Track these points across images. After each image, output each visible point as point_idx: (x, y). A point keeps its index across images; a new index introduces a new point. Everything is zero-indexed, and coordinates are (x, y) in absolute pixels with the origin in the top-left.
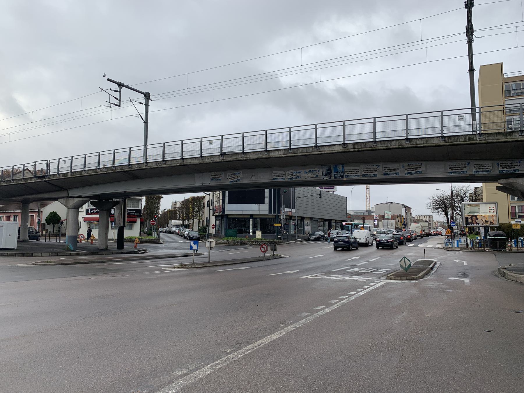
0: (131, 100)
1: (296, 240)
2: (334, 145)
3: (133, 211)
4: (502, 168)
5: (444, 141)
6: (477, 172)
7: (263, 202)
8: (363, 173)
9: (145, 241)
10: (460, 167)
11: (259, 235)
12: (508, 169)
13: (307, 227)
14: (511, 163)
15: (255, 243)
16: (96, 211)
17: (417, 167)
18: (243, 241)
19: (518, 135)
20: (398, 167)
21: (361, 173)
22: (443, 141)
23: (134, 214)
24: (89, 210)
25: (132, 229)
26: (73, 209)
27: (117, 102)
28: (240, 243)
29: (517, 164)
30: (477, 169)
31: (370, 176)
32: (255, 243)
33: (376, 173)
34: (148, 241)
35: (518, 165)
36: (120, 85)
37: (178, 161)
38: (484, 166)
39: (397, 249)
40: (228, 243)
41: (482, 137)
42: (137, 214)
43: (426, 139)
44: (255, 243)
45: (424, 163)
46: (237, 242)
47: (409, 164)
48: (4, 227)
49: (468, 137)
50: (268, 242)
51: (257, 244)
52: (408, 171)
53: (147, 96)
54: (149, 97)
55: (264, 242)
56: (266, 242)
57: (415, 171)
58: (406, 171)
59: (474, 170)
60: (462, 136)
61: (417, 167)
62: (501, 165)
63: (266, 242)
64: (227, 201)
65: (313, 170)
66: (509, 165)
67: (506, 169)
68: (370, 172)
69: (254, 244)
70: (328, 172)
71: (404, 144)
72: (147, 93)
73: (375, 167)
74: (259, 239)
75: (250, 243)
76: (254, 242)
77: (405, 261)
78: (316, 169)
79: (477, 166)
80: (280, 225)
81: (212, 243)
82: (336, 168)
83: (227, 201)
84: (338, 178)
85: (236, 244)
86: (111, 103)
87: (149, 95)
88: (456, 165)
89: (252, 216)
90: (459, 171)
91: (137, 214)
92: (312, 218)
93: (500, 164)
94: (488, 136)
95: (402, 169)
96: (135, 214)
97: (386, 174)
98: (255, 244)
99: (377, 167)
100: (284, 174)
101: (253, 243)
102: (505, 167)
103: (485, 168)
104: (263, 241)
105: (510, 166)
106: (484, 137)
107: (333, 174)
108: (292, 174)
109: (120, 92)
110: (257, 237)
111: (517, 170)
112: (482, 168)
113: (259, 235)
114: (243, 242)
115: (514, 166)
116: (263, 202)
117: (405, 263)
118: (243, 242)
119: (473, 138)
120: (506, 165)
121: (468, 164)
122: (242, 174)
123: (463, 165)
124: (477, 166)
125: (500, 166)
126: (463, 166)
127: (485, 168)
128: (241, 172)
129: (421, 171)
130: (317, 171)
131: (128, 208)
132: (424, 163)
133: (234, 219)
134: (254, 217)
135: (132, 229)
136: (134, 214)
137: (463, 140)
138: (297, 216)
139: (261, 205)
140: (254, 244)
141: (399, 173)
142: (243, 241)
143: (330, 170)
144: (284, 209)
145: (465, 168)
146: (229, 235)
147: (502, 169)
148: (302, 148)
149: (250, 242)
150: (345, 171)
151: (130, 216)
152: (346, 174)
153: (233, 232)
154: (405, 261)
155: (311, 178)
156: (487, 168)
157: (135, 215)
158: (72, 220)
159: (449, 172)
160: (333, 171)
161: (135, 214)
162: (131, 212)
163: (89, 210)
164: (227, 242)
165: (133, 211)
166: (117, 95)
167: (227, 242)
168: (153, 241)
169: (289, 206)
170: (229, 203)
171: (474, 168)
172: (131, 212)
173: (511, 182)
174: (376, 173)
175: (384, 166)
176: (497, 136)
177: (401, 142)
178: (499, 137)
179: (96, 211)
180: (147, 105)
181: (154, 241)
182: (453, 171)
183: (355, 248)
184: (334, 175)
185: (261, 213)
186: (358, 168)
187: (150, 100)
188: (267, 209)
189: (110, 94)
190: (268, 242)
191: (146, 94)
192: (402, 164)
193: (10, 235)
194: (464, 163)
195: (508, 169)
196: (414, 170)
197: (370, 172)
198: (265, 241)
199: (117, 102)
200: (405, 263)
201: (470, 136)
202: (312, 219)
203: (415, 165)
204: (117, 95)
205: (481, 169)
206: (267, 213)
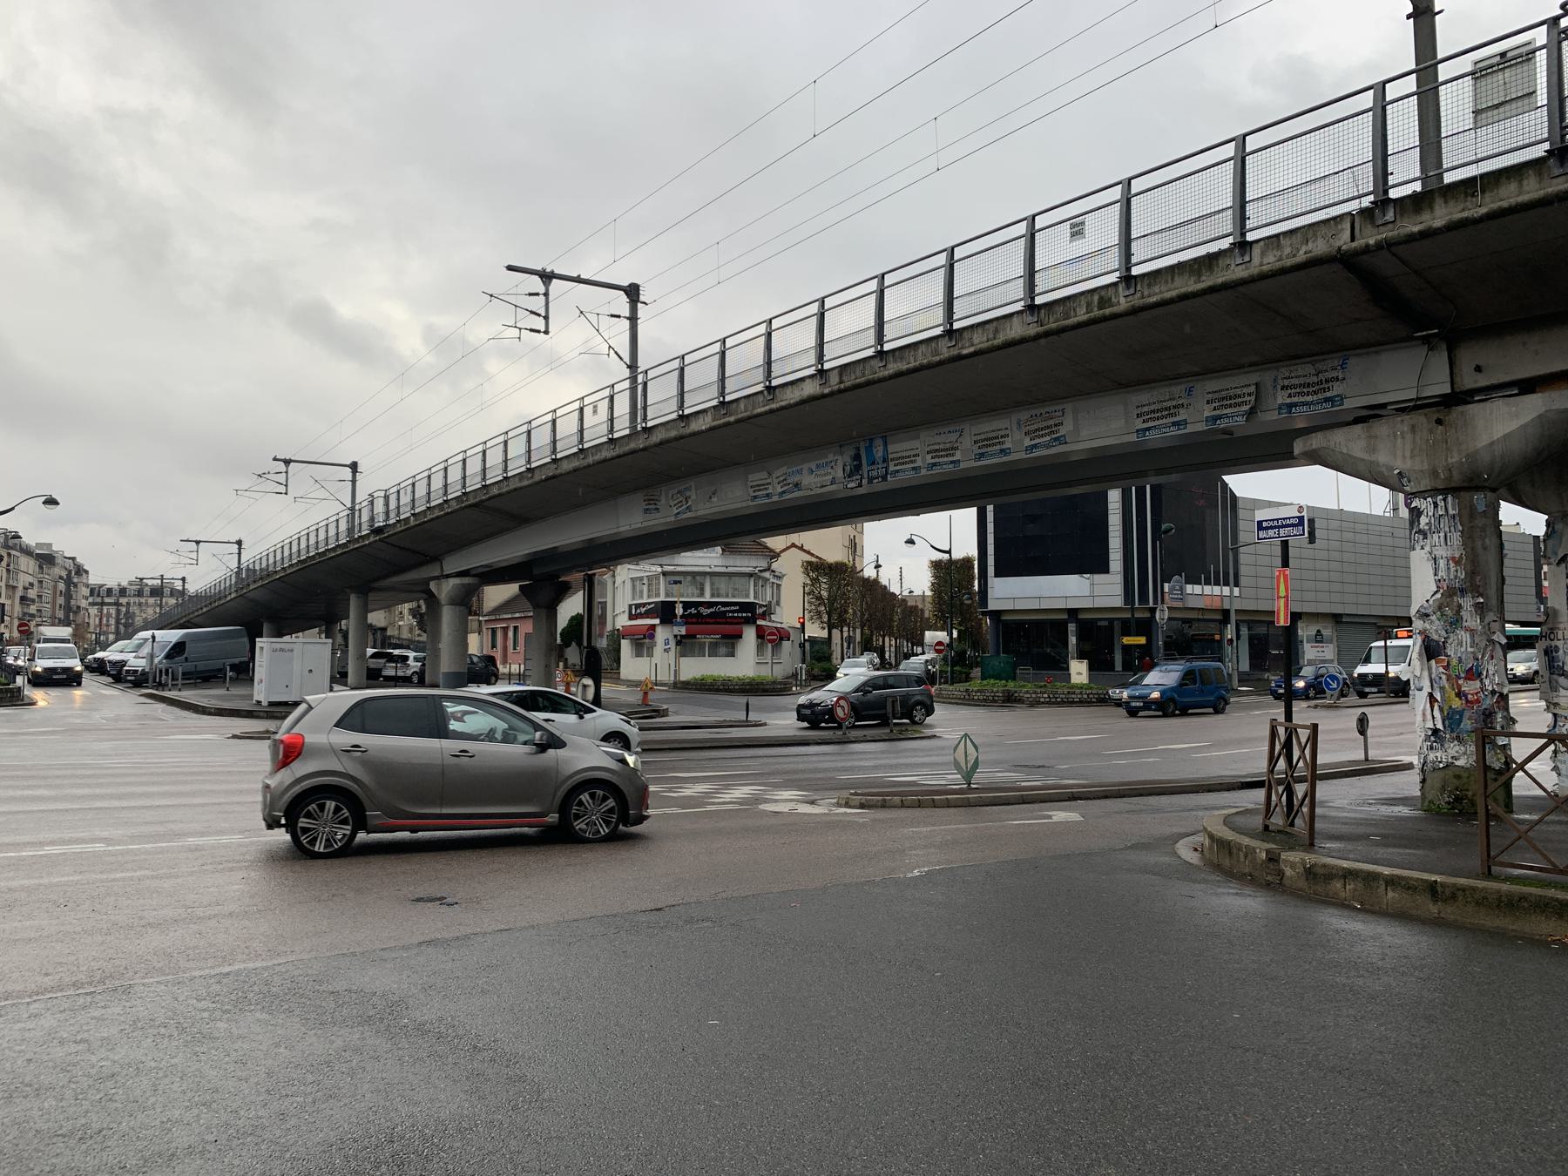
0: (581, 312)
1: (1233, 689)
2: (802, 380)
3: (733, 608)
4: (1290, 396)
5: (1037, 322)
6: (1215, 419)
7: (1105, 569)
8: (929, 459)
9: (737, 687)
10: (1166, 409)
11: (1080, 674)
12: (1309, 398)
13: (1316, 647)
14: (1314, 372)
15: (1049, 697)
16: (712, 610)
17: (1051, 422)
18: (1016, 692)
19: (1233, 262)
20: (1007, 429)
21: (924, 460)
22: (1035, 324)
23: (736, 615)
24: (633, 607)
25: (732, 654)
26: (457, 607)
27: (541, 326)
28: (1002, 699)
29: (1334, 374)
30: (1215, 409)
31: (944, 466)
32: (1049, 697)
33: (958, 456)
34: (748, 687)
35: (1340, 377)
36: (547, 277)
37: (549, 469)
38: (1236, 396)
39: (78, 688)
40: (967, 697)
41: (1132, 291)
42: (744, 615)
43: (995, 324)
44: (1048, 700)
45: (1069, 407)
46: (992, 694)
47: (1032, 416)
48: (295, 652)
49: (1096, 298)
50: (1091, 696)
51: (1054, 703)
52: (1031, 440)
53: (632, 292)
54: (638, 295)
55: (1079, 696)
56: (1085, 696)
57: (1048, 438)
58: (1027, 442)
59: (1206, 414)
60: (1083, 297)
61: (1051, 422)
62: (1286, 383)
63: (1085, 696)
64: (991, 570)
65: (824, 461)
66: (1308, 380)
67: (1302, 399)
68: (943, 453)
69: (1043, 703)
70: (855, 466)
71: (945, 350)
72: (630, 285)
73: (953, 437)
74: (1081, 687)
75: (1031, 699)
76: (1046, 695)
77: (965, 745)
78: (831, 457)
79: (1216, 396)
80: (1142, 640)
81: (588, 689)
82: (869, 449)
83: (991, 570)
84: (876, 481)
85: (991, 701)
86: (520, 329)
87: (638, 290)
88: (1154, 403)
89: (1073, 613)
90: (1164, 421)
91: (744, 615)
92: (1340, 615)
93: (1281, 383)
94: (1149, 285)
95: (1018, 435)
96: (740, 615)
97: (982, 455)
98: (1047, 703)
99: (958, 434)
100: (769, 481)
101: (1042, 700)
102: (1298, 390)
103: (1240, 400)
104: (1074, 693)
105: (1314, 384)
106: (1139, 288)
107: (865, 468)
108: (785, 480)
109: (546, 294)
110: (1072, 681)
111: (1338, 396)
112: (1228, 402)
113: (1080, 674)
114: (1016, 695)
115: (1327, 381)
116: (1105, 569)
117: (966, 752)
118: (1016, 695)
119: (1111, 299)
120: (1302, 381)
121: (1190, 392)
122: (694, 491)
123: (1174, 399)
124: (1216, 396)
125: (1282, 388)
126: (1174, 403)
127: (1240, 400)
128: (693, 484)
129: (1064, 436)
130: (833, 464)
131: (600, 600)
132: (1070, 404)
133: (1020, 624)
134: (1081, 616)
135: (732, 654)
136: (736, 615)
137: (1085, 310)
138: (1236, 610)
139: (1098, 578)
140: (1043, 703)
141: (1009, 449)
142: (1016, 692)
143: (857, 457)
144: (1181, 589)
145: (1182, 411)
146: (991, 673)
147: (1289, 401)
148: (745, 397)
149: (1034, 695)
150: (890, 456)
151: (724, 620)
152: (892, 468)
153: (1002, 665)
154: (965, 745)
155: (823, 486)
156: (1244, 400)
157: (738, 617)
158: (449, 634)
159: (1138, 431)
160: (864, 461)
161: (740, 615)
162: (728, 609)
163: (633, 607)
164: (964, 694)
165: (733, 608)
166: (538, 304)
167: (964, 694)
168: (762, 687)
169: (1217, 573)
170: (996, 575)
171: (1206, 407)
172: (728, 609)
173: (1314, 447)
174: (958, 456)
175: (975, 430)
176: (1173, 280)
177: (938, 345)
178: (1178, 281)
179: (712, 610)
180: (633, 319)
181: (768, 687)
182: (1151, 424)
183: (1211, 710)
184: (868, 471)
185: (1099, 603)
186: (915, 444)
187: (642, 303)
188: (1119, 589)
189: (516, 306)
190: (1091, 696)
191: (628, 289)
192: (1014, 418)
193: (310, 671)
194: (1177, 390)
195: (1309, 398)
196: (1046, 435)
197: (943, 453)
198: (1081, 693)
199: (539, 324)
200: (966, 752)
201: (1103, 293)
202: (1339, 620)
203: (1048, 415)
204: (538, 304)
205: (1226, 407)
206: (1118, 602)
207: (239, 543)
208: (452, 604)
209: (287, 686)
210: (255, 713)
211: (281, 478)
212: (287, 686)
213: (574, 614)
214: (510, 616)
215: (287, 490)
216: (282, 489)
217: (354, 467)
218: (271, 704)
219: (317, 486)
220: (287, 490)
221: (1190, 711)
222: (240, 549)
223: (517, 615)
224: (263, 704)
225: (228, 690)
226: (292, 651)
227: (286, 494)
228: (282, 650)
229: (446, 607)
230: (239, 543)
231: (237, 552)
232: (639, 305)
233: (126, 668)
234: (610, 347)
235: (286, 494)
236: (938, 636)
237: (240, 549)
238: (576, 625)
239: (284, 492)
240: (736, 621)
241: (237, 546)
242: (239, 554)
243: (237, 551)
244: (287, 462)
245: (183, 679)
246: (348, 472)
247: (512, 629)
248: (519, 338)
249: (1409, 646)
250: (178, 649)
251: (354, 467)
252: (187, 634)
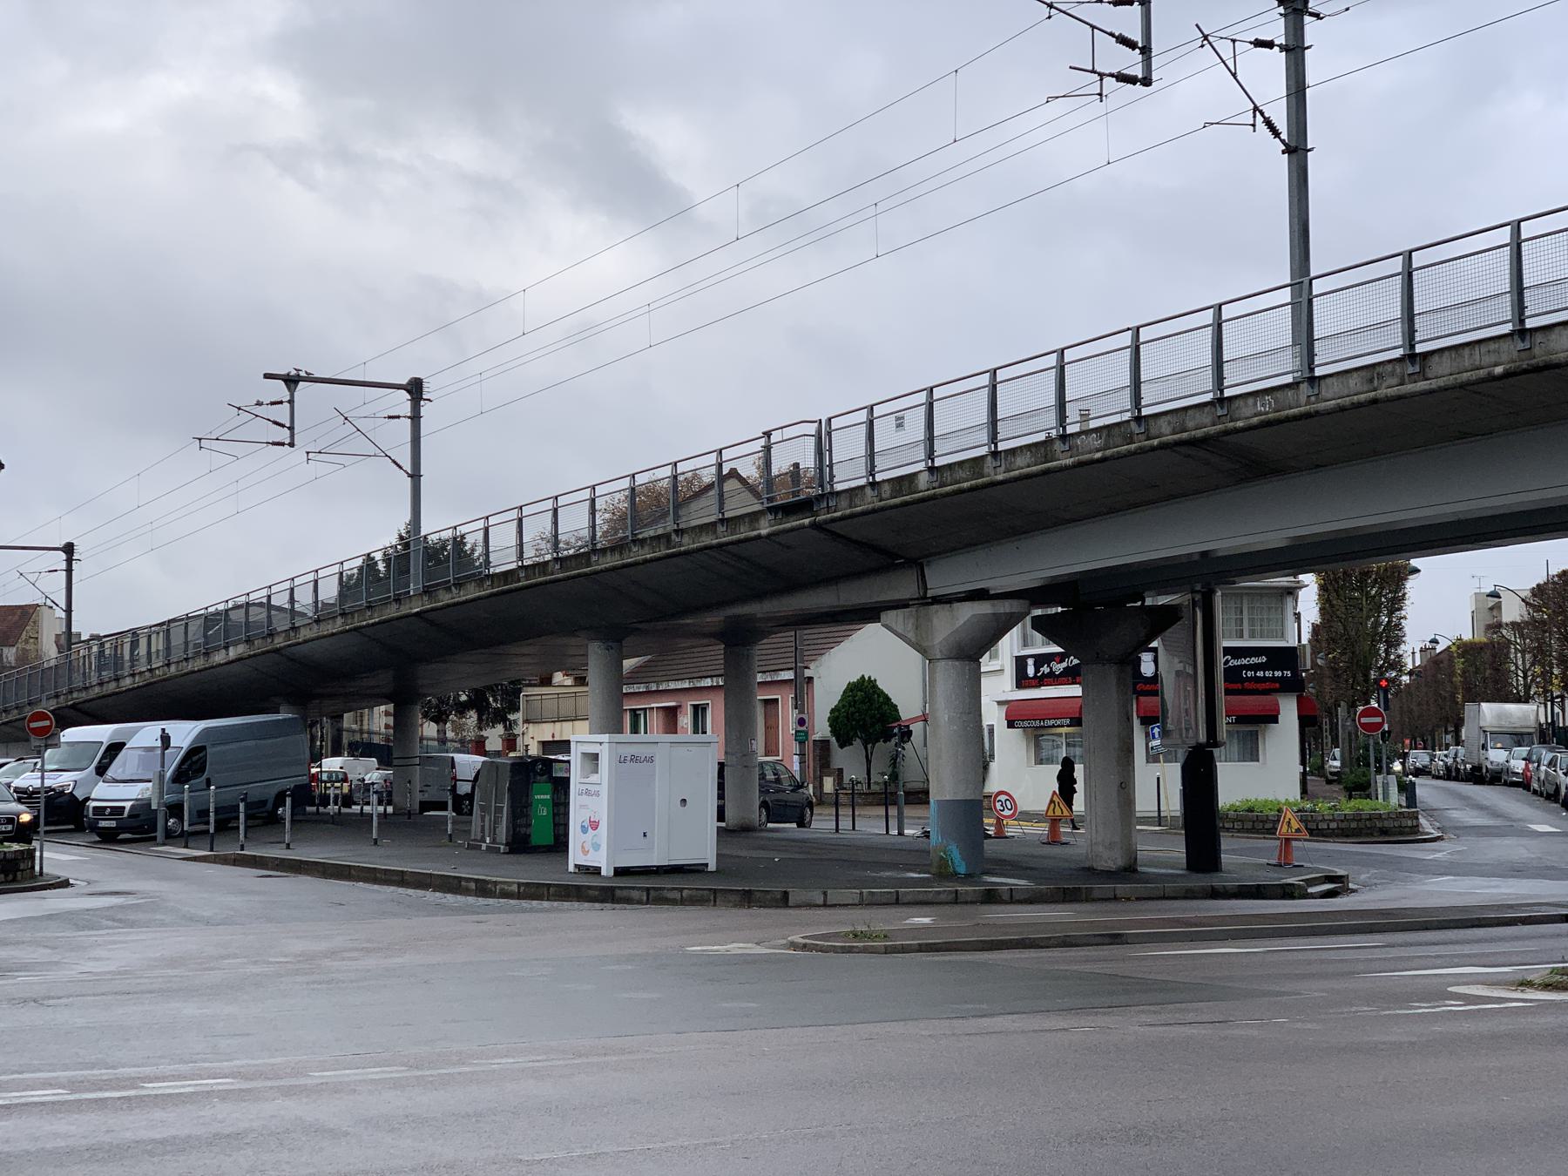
3: (1254, 660)
9: (1333, 825)
24: (1030, 662)
34: (1354, 825)
37: (1497, 352)
42: (1278, 674)
48: (657, 759)
91: (1278, 674)
96: (1269, 674)
157: (1265, 679)
161: (1269, 674)
162: (1245, 661)
163: (1030, 662)
165: (1254, 660)
168: (1379, 824)
172: (1245, 661)
181: (1323, 826)
187: (1312, 14)
189: (1093, 27)
207: (69, 549)
208: (957, 658)
209: (645, 835)
210: (618, 893)
211: (282, 413)
212: (645, 835)
213: (854, 679)
214: (686, 685)
215: (292, 436)
216: (284, 435)
217: (415, 389)
218: (620, 872)
219: (349, 428)
220: (292, 436)
221: (122, 836)
222: (69, 561)
223: (708, 682)
224: (604, 873)
225: (288, 847)
226: (651, 760)
227: (292, 445)
228: (634, 759)
229: (943, 663)
230: (69, 549)
231: (64, 567)
232: (1307, 19)
233: (92, 804)
234: (1256, 109)
235: (292, 445)
236: (1508, 715)
237: (69, 561)
238: (863, 702)
239: (287, 441)
240: (1259, 686)
241: (64, 556)
242: (69, 571)
243: (64, 565)
244: (291, 381)
245: (46, 825)
246: (401, 402)
247: (689, 710)
248: (1100, 94)
249: (102, 743)
250: (193, 763)
251: (415, 389)
252: (206, 731)
